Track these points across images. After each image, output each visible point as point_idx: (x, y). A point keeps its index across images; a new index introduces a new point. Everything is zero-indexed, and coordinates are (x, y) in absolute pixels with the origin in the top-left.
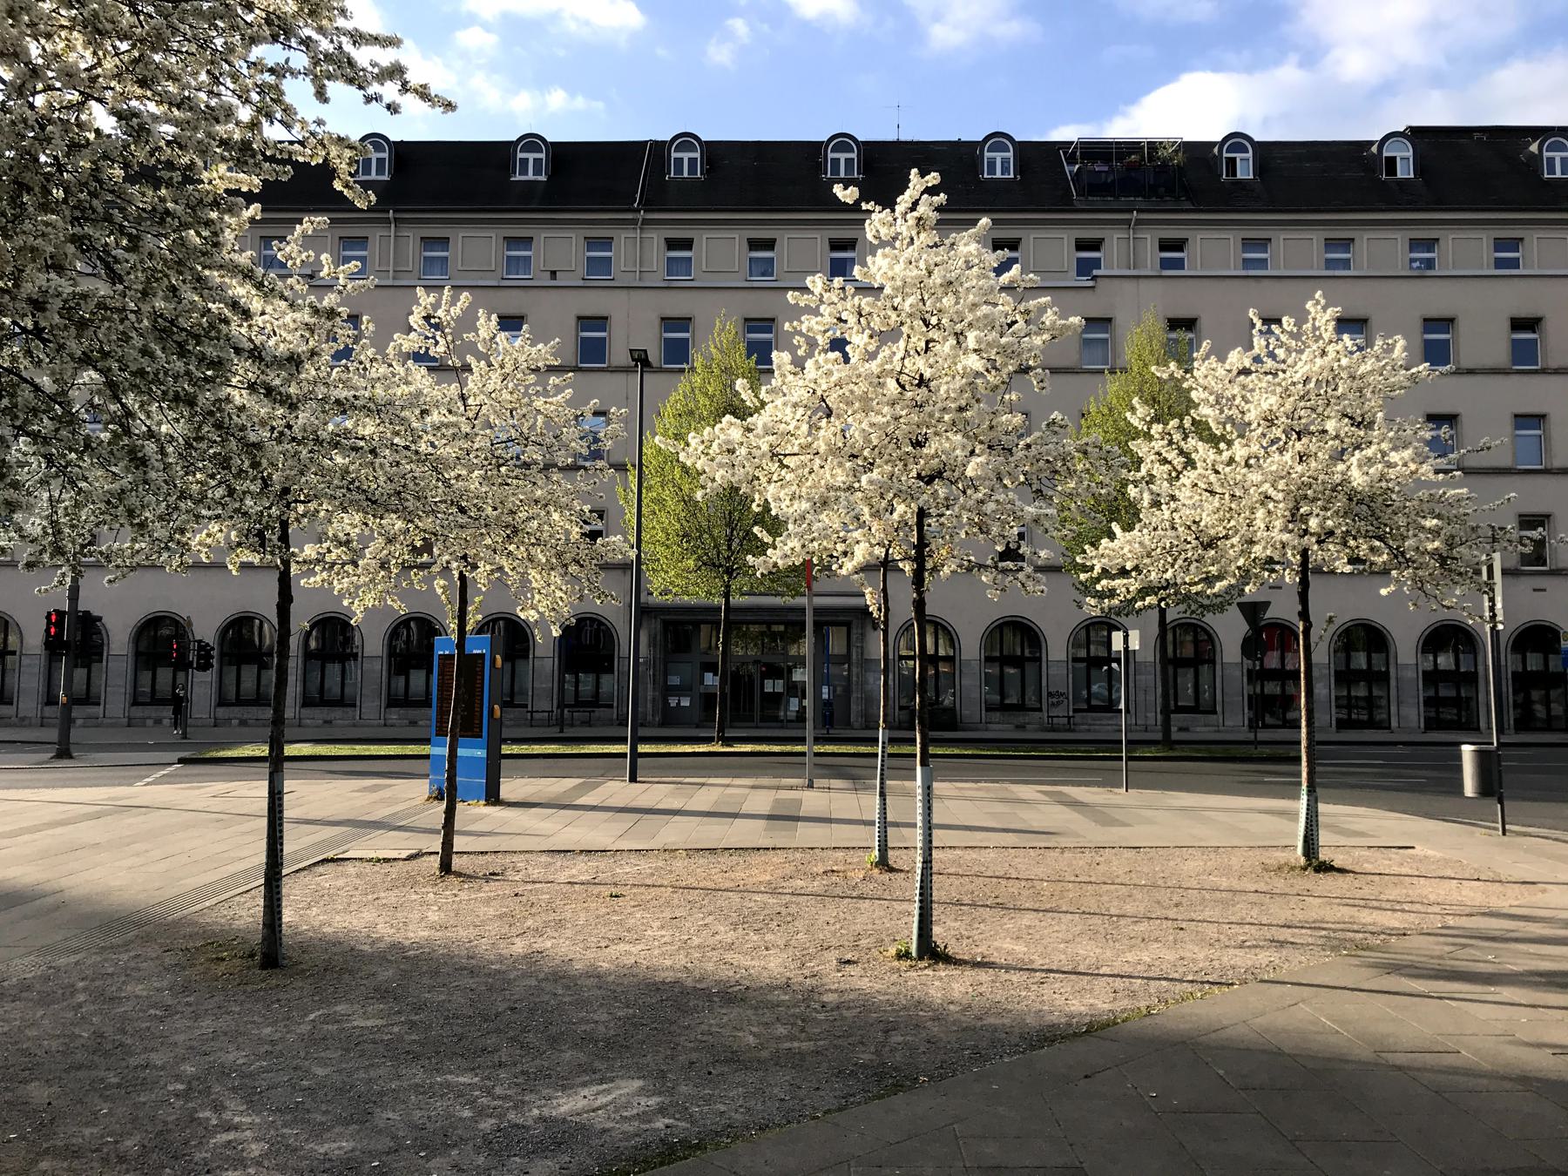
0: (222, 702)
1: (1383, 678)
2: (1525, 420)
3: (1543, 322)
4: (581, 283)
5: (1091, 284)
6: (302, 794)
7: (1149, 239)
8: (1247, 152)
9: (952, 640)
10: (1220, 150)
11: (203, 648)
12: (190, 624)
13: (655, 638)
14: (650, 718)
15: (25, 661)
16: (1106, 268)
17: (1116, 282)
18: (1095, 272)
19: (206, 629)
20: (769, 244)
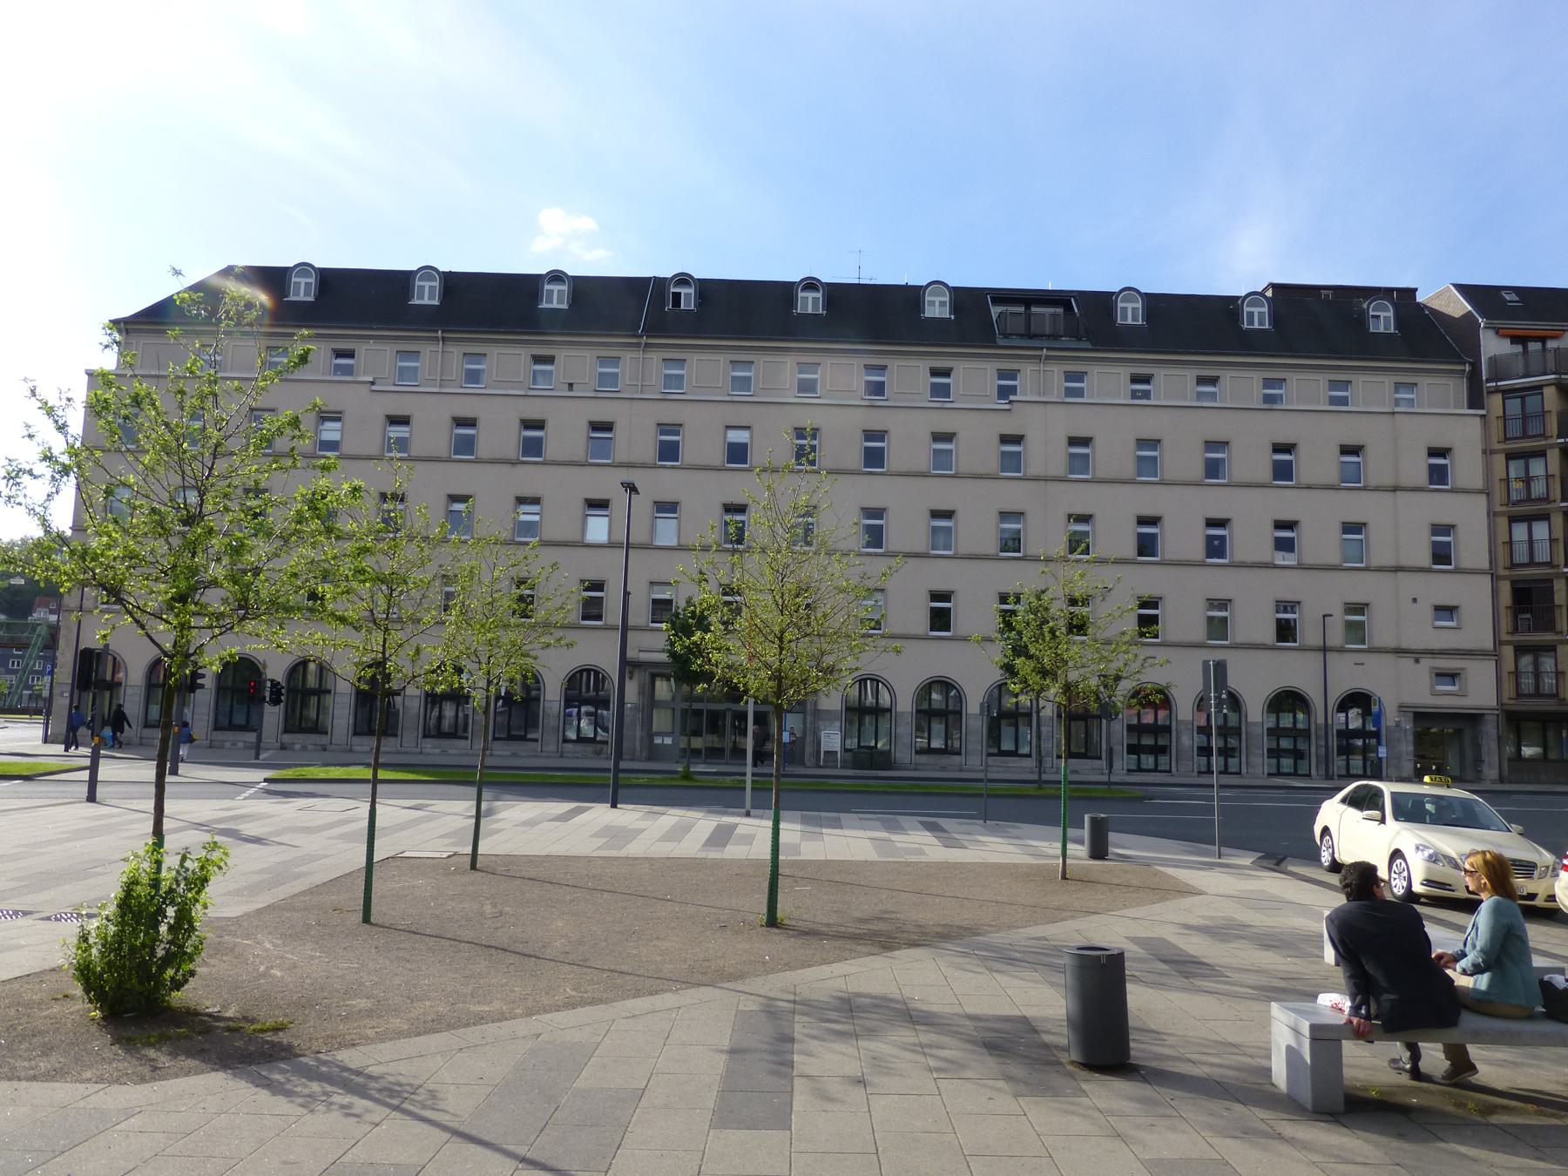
0: (217, 727)
1: (1167, 729)
2: (1352, 528)
3: (1297, 446)
4: (592, 394)
5: (1007, 407)
6: (389, 812)
7: (1056, 371)
8: (1138, 302)
9: (960, 698)
10: (924, 293)
11: (275, 684)
12: (265, 666)
13: (644, 687)
14: (638, 753)
15: (129, 691)
16: (1220, 402)
17: (1028, 406)
18: (1012, 398)
19: (276, 671)
20: (946, 373)
